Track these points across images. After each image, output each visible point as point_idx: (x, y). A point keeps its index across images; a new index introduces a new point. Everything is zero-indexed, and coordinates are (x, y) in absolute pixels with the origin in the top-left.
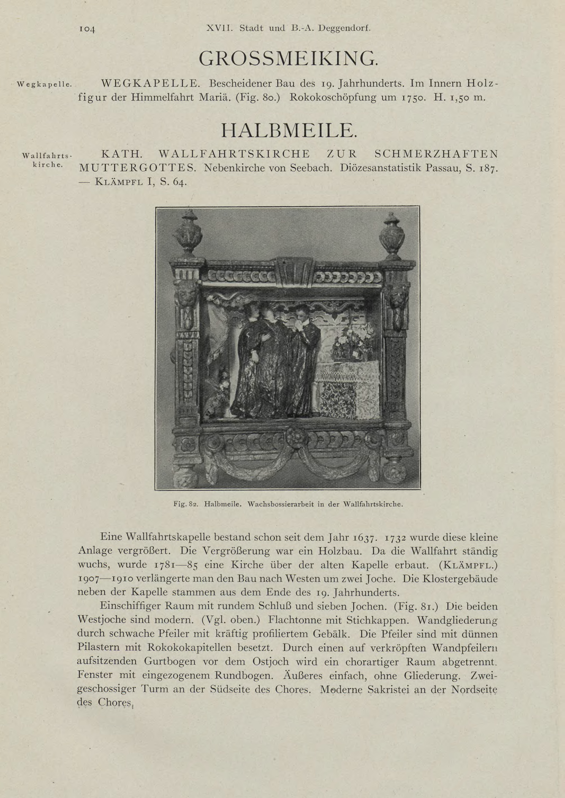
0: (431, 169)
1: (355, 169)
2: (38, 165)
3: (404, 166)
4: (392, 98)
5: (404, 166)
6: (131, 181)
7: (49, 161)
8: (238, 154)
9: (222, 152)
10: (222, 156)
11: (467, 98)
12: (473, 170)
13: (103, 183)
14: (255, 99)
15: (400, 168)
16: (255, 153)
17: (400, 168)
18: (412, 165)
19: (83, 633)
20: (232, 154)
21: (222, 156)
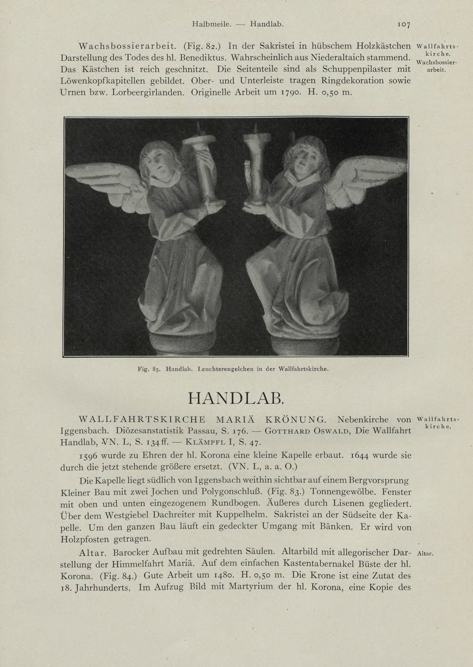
0: (192, 432)
1: (128, 431)
2: (429, 54)
3: (169, 429)
4: (273, 92)
5: (169, 429)
6: (216, 442)
7: (439, 423)
8: (145, 419)
9: (132, 418)
10: (132, 420)
11: (336, 93)
12: (227, 433)
13: (192, 443)
14: (200, 48)
15: (166, 431)
16: (160, 419)
17: (166, 431)
18: (176, 429)
19: (309, 503)
20: (140, 419)
21: (132, 420)
